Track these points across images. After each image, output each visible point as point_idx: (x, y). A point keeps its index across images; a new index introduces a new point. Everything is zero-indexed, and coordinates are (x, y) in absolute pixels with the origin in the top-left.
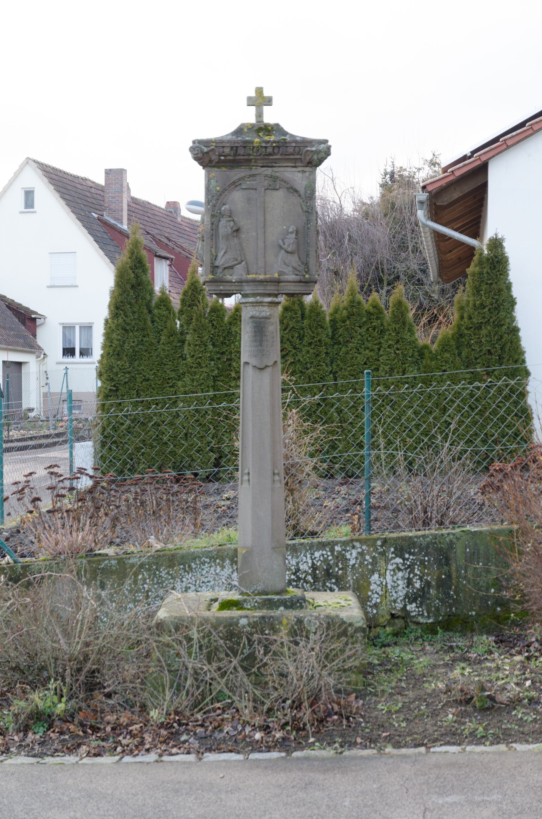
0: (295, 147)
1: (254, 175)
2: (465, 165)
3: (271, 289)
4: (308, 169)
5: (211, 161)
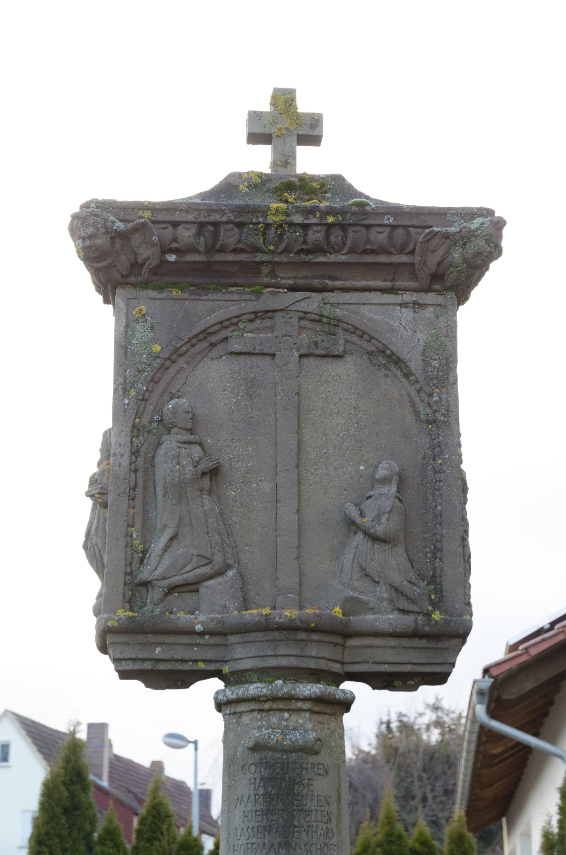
0: (394, 227)
1: (268, 314)
2: (543, 640)
3: (318, 653)
4: (430, 298)
5: (136, 266)
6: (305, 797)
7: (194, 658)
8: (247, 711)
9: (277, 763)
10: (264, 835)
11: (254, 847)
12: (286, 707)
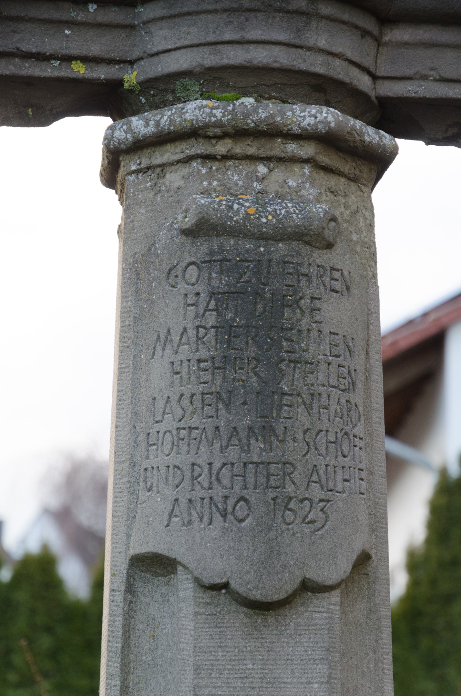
6: (305, 334)
7: (64, 52)
8: (178, 162)
9: (247, 261)
10: (217, 411)
11: (193, 436)
12: (263, 153)
